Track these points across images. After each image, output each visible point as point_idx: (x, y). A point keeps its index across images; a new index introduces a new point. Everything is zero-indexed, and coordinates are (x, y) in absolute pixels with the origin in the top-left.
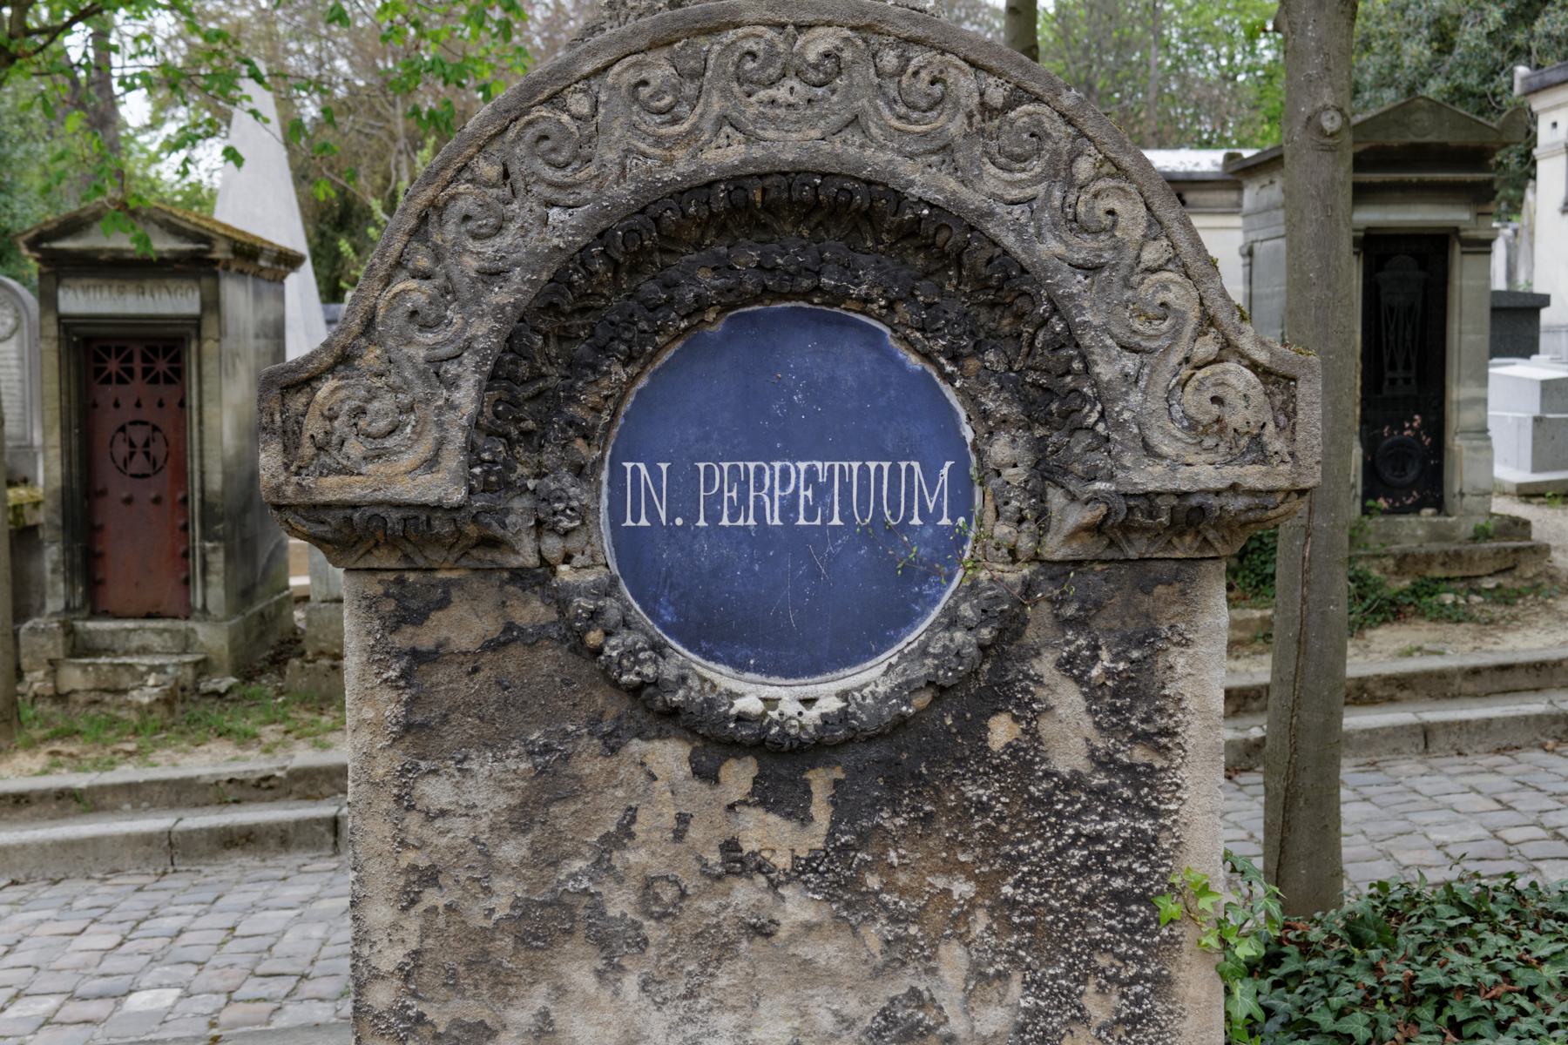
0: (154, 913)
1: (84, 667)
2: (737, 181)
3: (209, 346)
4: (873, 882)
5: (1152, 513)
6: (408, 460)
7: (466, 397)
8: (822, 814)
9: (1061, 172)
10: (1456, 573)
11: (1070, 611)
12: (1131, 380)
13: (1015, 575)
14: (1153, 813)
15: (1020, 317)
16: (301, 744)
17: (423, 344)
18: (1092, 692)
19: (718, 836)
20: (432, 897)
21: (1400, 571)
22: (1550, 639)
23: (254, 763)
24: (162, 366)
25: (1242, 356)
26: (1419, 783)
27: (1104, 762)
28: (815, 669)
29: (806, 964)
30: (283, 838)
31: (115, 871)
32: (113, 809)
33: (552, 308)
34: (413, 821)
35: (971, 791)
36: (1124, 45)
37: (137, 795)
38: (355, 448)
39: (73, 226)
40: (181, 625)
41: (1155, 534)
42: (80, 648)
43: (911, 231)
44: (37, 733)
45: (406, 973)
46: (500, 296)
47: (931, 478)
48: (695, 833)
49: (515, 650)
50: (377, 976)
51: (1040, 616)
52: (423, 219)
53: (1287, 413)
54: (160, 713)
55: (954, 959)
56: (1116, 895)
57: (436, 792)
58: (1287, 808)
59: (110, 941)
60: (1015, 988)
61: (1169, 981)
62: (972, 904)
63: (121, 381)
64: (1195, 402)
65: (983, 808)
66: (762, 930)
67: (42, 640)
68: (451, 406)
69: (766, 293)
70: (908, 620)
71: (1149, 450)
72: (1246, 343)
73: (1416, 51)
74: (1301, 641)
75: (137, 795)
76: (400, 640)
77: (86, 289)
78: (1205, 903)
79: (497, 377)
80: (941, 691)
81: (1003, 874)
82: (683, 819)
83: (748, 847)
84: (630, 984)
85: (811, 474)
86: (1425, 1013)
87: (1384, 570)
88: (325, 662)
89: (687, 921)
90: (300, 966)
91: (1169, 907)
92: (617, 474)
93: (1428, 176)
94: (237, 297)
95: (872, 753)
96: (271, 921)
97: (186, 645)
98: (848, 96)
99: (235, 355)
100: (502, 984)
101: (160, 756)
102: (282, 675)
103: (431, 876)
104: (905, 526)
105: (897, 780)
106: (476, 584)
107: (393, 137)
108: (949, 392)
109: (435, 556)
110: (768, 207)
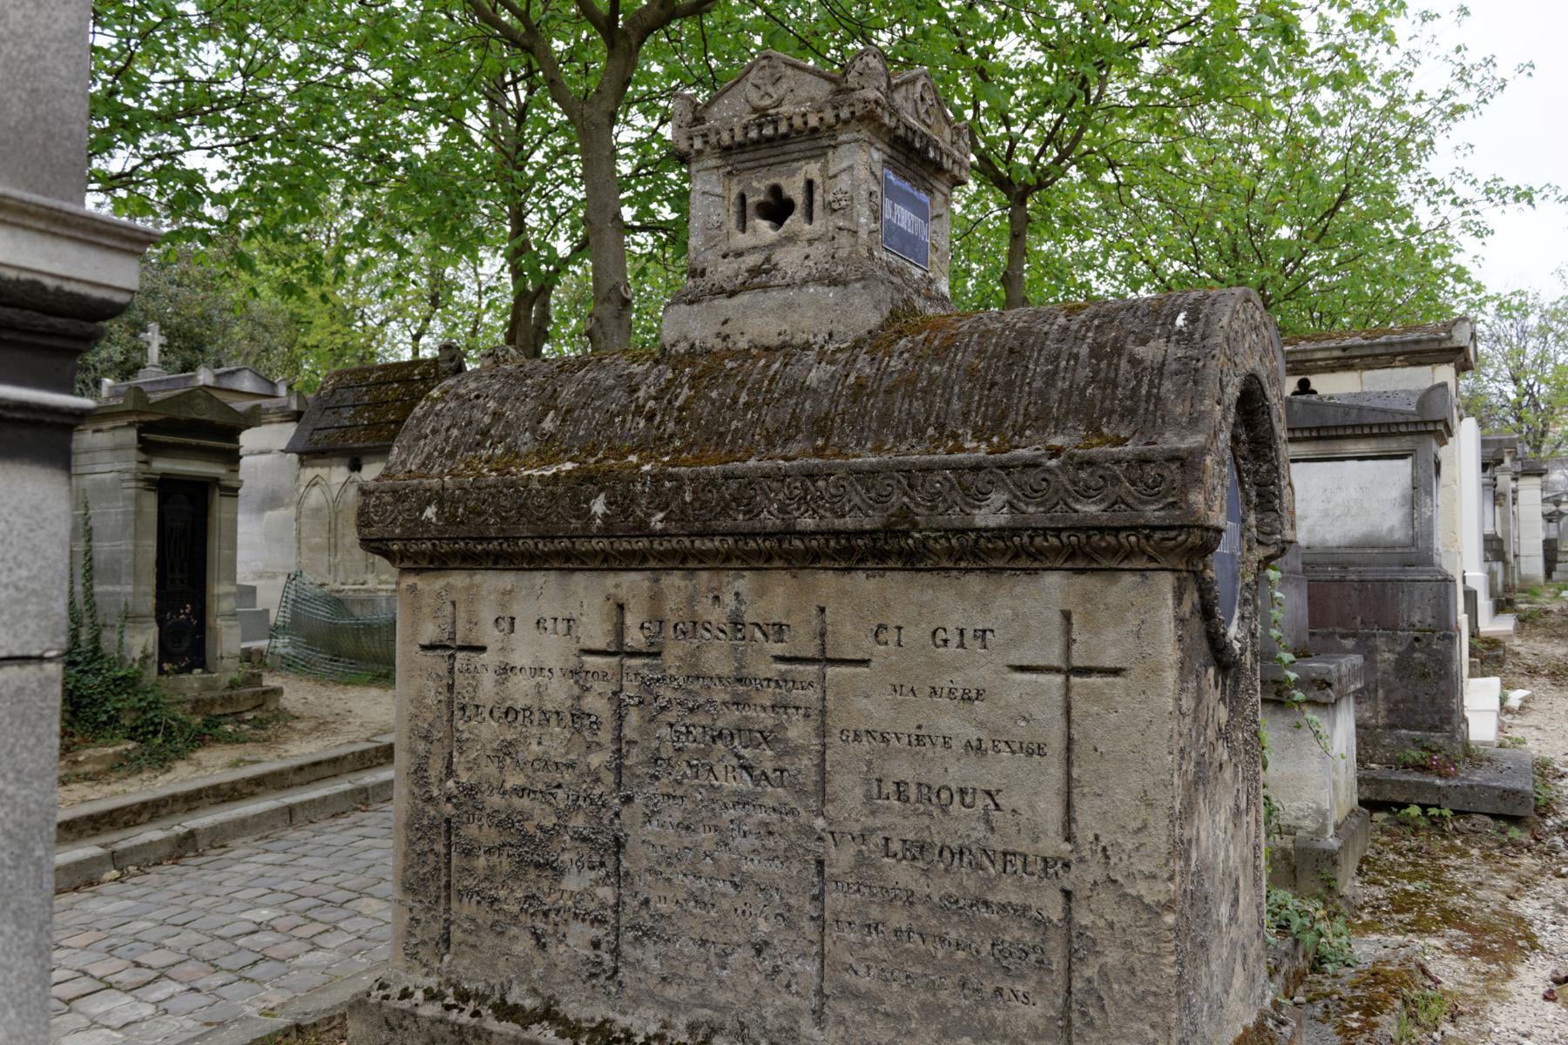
10: (229, 711)
21: (194, 711)
22: (320, 743)
87: (184, 712)
93: (203, 442)
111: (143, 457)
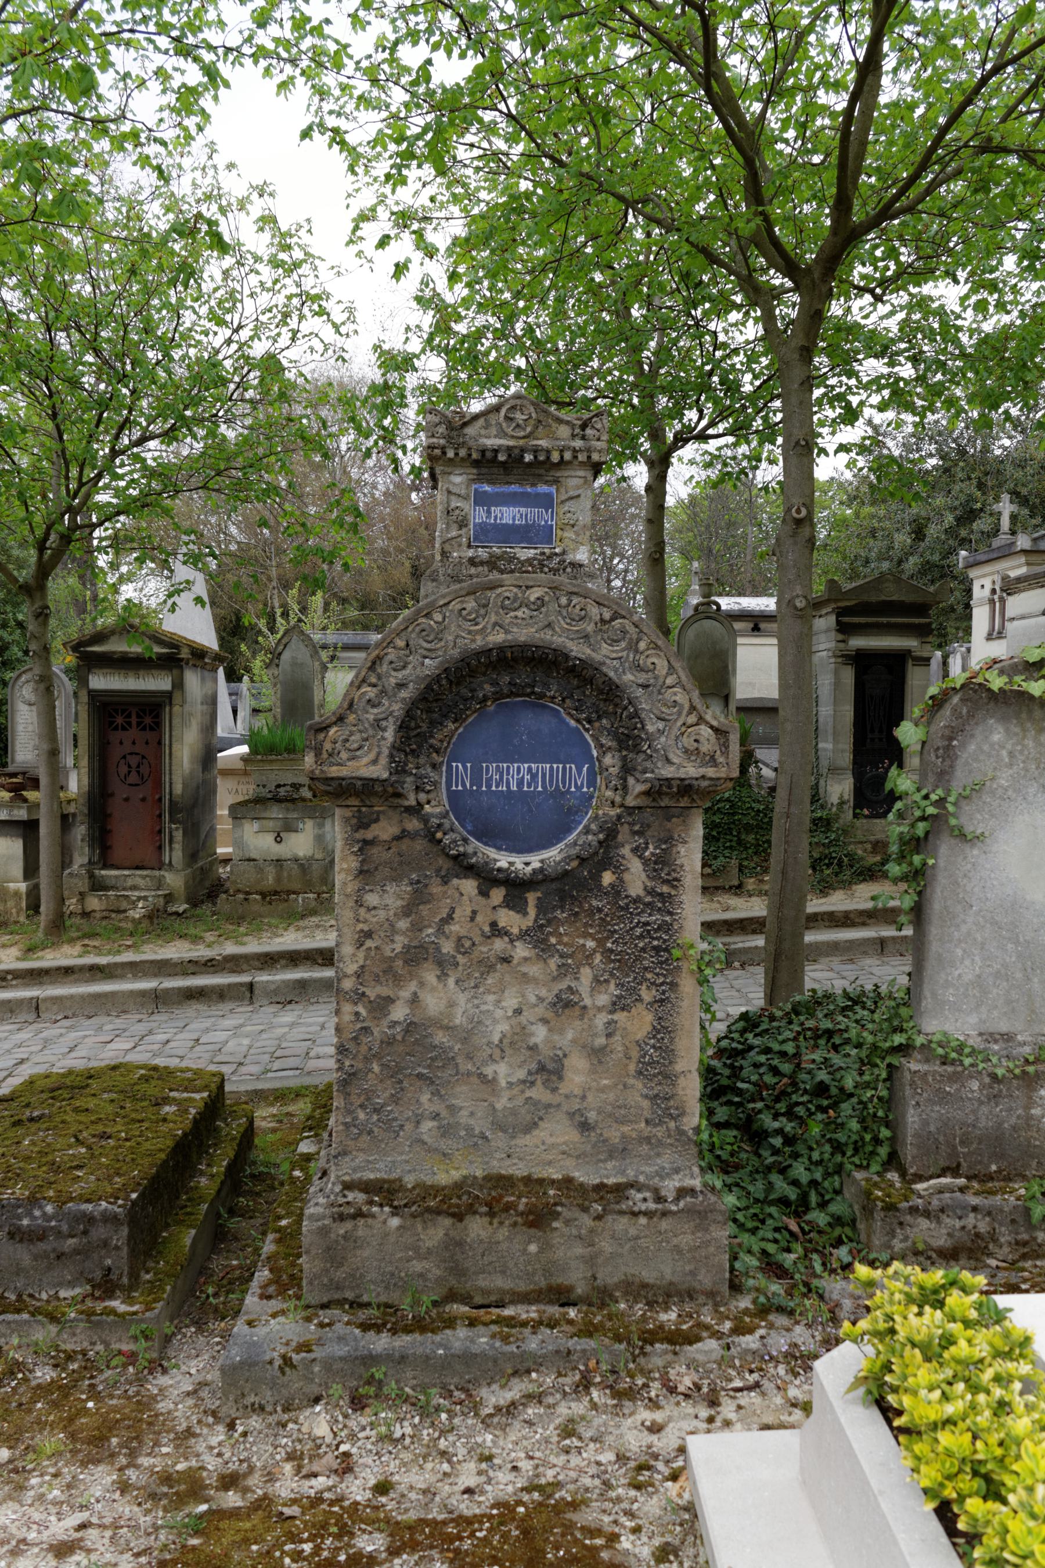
0: (151, 1032)
1: (100, 897)
2: (501, 649)
3: (176, 709)
4: (553, 940)
5: (670, 787)
6: (365, 760)
7: (390, 735)
8: (532, 911)
9: (633, 647)
11: (637, 828)
12: (661, 732)
13: (613, 812)
14: (671, 914)
15: (616, 705)
16: (228, 943)
17: (372, 713)
18: (646, 862)
19: (489, 920)
20: (369, 943)
23: (201, 952)
24: (148, 720)
25: (707, 723)
26: (875, 970)
27: (650, 892)
28: (530, 850)
29: (525, 974)
30: (221, 994)
31: (124, 1012)
32: (122, 977)
33: (425, 699)
34: (362, 911)
35: (595, 903)
36: (731, 525)
37: (135, 969)
38: (344, 755)
39: (100, 637)
40: (157, 873)
41: (672, 796)
42: (97, 886)
43: (572, 670)
44: (75, 935)
45: (358, 975)
46: (404, 694)
47: (579, 771)
48: (479, 918)
49: (406, 841)
50: (346, 976)
51: (624, 832)
52: (374, 663)
53: (725, 746)
54: (145, 924)
55: (586, 974)
56: (654, 948)
57: (372, 899)
58: (776, 960)
59: (128, 1046)
60: (612, 986)
61: (677, 985)
62: (594, 951)
63: (124, 729)
64: (687, 742)
65: (600, 910)
66: (506, 960)
67: (75, 881)
68: (383, 738)
69: (512, 694)
70: (569, 830)
71: (668, 761)
72: (708, 717)
73: (903, 539)
74: (784, 873)
75: (135, 969)
76: (358, 835)
77: (105, 675)
78: (692, 952)
79: (403, 727)
80: (583, 860)
81: (608, 938)
82: (474, 912)
83: (501, 924)
84: (451, 981)
85: (530, 769)
86: (822, 1042)
88: (241, 896)
89: (475, 955)
90: (239, 1058)
91: (676, 953)
92: (449, 768)
93: (893, 620)
94: (192, 680)
95: (554, 886)
96: (220, 1036)
97: (159, 884)
98: (547, 615)
99: (191, 714)
100: (398, 980)
101: (146, 948)
102: (215, 904)
103: (369, 935)
104: (568, 791)
105: (565, 898)
106: (390, 813)
107: (270, 580)
108: (587, 736)
109: (375, 800)
110: (514, 659)
111: (841, 637)
